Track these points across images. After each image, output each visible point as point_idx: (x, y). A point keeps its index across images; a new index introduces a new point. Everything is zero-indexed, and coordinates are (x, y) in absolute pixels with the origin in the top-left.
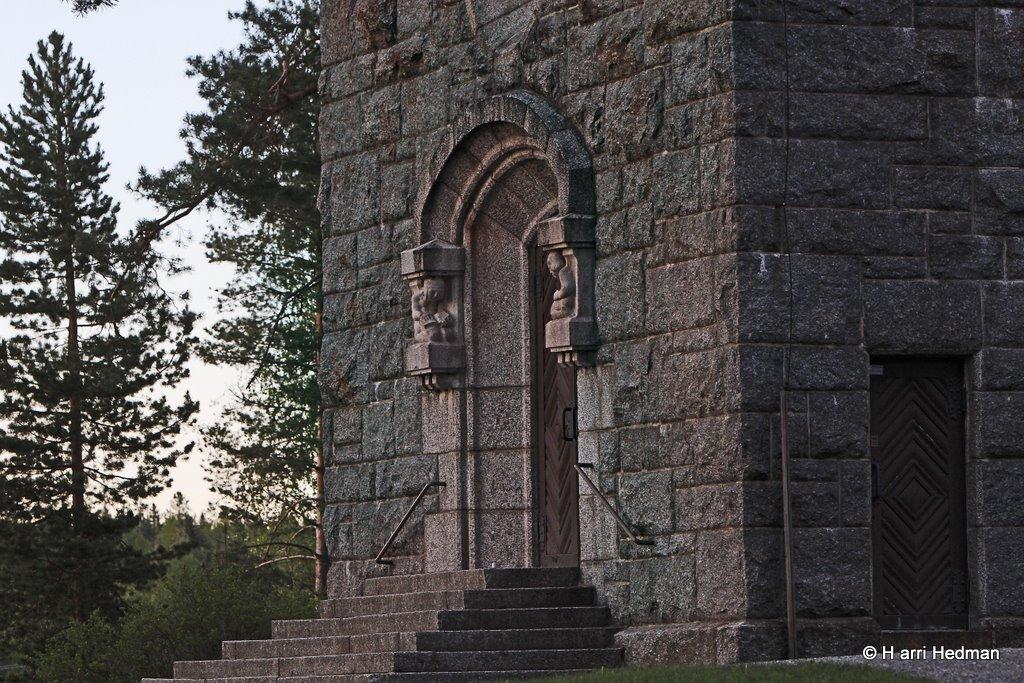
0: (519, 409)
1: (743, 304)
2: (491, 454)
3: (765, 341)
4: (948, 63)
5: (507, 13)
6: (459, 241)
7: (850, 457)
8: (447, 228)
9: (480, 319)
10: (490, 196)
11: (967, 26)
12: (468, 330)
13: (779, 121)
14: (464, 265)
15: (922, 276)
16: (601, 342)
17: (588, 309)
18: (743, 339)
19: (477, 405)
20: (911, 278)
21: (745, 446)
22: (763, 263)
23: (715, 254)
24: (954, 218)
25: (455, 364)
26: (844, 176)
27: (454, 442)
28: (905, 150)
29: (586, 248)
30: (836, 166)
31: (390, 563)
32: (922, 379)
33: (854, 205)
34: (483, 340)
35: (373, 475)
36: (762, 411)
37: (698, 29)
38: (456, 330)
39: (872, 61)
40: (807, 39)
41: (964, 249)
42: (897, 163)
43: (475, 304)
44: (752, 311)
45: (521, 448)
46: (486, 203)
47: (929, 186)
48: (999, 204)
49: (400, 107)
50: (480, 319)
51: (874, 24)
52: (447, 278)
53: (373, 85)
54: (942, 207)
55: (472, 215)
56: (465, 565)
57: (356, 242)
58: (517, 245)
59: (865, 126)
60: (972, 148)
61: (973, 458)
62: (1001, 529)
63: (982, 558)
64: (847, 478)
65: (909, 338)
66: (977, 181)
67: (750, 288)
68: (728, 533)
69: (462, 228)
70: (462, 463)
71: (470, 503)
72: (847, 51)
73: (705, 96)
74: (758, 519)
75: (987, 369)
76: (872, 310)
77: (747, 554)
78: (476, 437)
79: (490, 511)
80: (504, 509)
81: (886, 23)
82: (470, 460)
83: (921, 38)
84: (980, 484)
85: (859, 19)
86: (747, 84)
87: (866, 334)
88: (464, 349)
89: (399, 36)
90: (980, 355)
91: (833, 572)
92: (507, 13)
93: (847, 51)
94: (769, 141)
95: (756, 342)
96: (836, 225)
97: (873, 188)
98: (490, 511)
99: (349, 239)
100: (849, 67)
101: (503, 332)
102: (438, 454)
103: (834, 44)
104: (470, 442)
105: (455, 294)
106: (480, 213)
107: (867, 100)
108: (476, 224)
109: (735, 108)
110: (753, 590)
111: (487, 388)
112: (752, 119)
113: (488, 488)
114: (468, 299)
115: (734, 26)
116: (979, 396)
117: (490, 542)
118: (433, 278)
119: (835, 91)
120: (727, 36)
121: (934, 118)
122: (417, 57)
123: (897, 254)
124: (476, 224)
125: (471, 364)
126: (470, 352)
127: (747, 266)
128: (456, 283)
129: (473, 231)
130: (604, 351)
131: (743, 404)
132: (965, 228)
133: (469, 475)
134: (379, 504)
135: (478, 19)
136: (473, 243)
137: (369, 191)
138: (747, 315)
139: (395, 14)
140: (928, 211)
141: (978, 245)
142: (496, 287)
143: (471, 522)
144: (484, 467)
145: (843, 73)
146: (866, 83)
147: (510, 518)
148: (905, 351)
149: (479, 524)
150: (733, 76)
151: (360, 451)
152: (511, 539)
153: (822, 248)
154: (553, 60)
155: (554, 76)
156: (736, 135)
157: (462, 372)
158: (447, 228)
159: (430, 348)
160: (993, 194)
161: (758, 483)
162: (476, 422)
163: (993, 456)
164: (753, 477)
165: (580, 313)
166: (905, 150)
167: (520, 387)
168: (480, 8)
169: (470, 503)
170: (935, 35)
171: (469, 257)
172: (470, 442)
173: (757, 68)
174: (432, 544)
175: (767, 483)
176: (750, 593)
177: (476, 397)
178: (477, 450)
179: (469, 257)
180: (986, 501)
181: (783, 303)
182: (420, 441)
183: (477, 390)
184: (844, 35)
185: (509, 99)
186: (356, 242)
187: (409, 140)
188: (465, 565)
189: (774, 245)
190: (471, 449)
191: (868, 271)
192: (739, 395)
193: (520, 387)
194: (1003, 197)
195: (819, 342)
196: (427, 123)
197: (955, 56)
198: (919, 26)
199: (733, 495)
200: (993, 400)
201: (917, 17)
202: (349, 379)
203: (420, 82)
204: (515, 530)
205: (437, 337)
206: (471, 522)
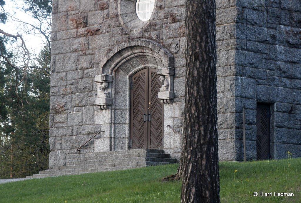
0: (126, 114)
1: (236, 88)
2: (118, 125)
3: (240, 97)
4: (273, 37)
5: (131, 21)
6: (111, 74)
7: (253, 125)
8: (109, 71)
9: (116, 93)
10: (123, 64)
11: (275, 29)
12: (113, 96)
13: (243, 47)
14: (113, 80)
15: (266, 85)
16: (175, 97)
17: (173, 89)
18: (236, 96)
19: (115, 113)
20: (264, 85)
21: (236, 120)
22: (240, 79)
23: (226, 76)
24: (272, 72)
25: (111, 103)
26: (254, 61)
27: (109, 121)
28: (264, 56)
29: (172, 75)
30: (253, 58)
31: (79, 150)
32: (264, 107)
33: (255, 67)
34: (117, 98)
35: (72, 130)
36: (239, 113)
37: (221, 25)
38: (110, 95)
39: (260, 35)
40: (249, 28)
41: (274, 79)
42: (263, 59)
43: (115, 89)
44: (238, 90)
45: (126, 123)
46: (121, 66)
47: (268, 64)
48: (281, 70)
49: (88, 43)
50: (116, 93)
51: (260, 26)
52: (109, 82)
53: (76, 37)
54: (270, 70)
55: (116, 68)
56: (111, 150)
57: (67, 74)
58: (126, 76)
59: (258, 50)
60: (276, 57)
61: (273, 127)
62: (279, 144)
63: (275, 150)
64: (253, 129)
65: (264, 98)
66: (276, 64)
67: (238, 84)
68: (229, 141)
69: (112, 71)
70: (111, 126)
71: (112, 136)
72: (255, 32)
73: (223, 40)
74: (238, 138)
75: (277, 107)
76: (258, 92)
77: (236, 146)
78: (114, 120)
79: (117, 138)
80: (121, 138)
81: (262, 26)
82: (113, 126)
83: (268, 31)
84: (275, 133)
85: (257, 25)
86: (238, 37)
87: (257, 97)
88: (112, 100)
89: (88, 25)
90: (276, 104)
91: (251, 151)
92: (131, 21)
93: (255, 32)
94: (241, 51)
95: (238, 97)
96: (252, 71)
97: (259, 64)
98: (117, 138)
99: (64, 74)
100: (255, 36)
101: (122, 96)
102: (101, 124)
103: (253, 30)
104: (113, 121)
105: (110, 86)
106: (118, 68)
107: (258, 44)
108: (117, 71)
109: (236, 43)
110: (237, 154)
111: (118, 109)
112: (239, 46)
113: (117, 132)
114: (114, 88)
115: (236, 24)
116: (275, 113)
117: (117, 145)
118: (106, 82)
119: (253, 41)
120: (234, 26)
121: (270, 49)
122: (98, 30)
123: (262, 79)
124: (117, 71)
125: (114, 103)
126: (114, 100)
127: (237, 79)
128: (110, 84)
129: (115, 72)
130: (177, 99)
131: (236, 111)
132: (273, 75)
133: (113, 129)
134: (74, 137)
135: (124, 22)
136: (115, 75)
137: (74, 62)
138: (237, 90)
139: (87, 20)
140: (268, 70)
141: (276, 79)
142: (121, 86)
143: (113, 140)
144: (116, 127)
145: (254, 37)
146: (258, 40)
147: (123, 140)
148: (263, 101)
149: (115, 141)
150: (235, 35)
151: (67, 124)
152: (122, 145)
153: (250, 77)
154: (158, 31)
155: (158, 37)
156: (235, 49)
157: (112, 105)
158: (109, 71)
159: (106, 99)
160: (280, 68)
161: (237, 129)
162: (115, 117)
163: (278, 127)
164: (237, 128)
165: (170, 91)
166: (264, 56)
167: (126, 109)
168: (124, 19)
169: (112, 136)
170: (271, 30)
171: (114, 78)
172: (113, 121)
173: (240, 34)
174: (98, 146)
175: (239, 129)
176: (236, 154)
177: (115, 111)
178: (115, 124)
179: (114, 78)
180: (276, 137)
181: (243, 88)
182: (94, 121)
183: (115, 109)
184: (255, 28)
185: (142, 41)
186: (67, 74)
187: (92, 50)
188: (111, 150)
189: (242, 75)
190: (114, 123)
191: (257, 83)
192: (234, 109)
193: (126, 109)
194: (282, 68)
195: (248, 98)
196: (101, 46)
197: (274, 35)
198: (267, 28)
199: (232, 132)
200: (278, 114)
201: (267, 25)
202: (64, 107)
203: (97, 36)
204: (123, 143)
205: (107, 97)
206: (113, 140)
